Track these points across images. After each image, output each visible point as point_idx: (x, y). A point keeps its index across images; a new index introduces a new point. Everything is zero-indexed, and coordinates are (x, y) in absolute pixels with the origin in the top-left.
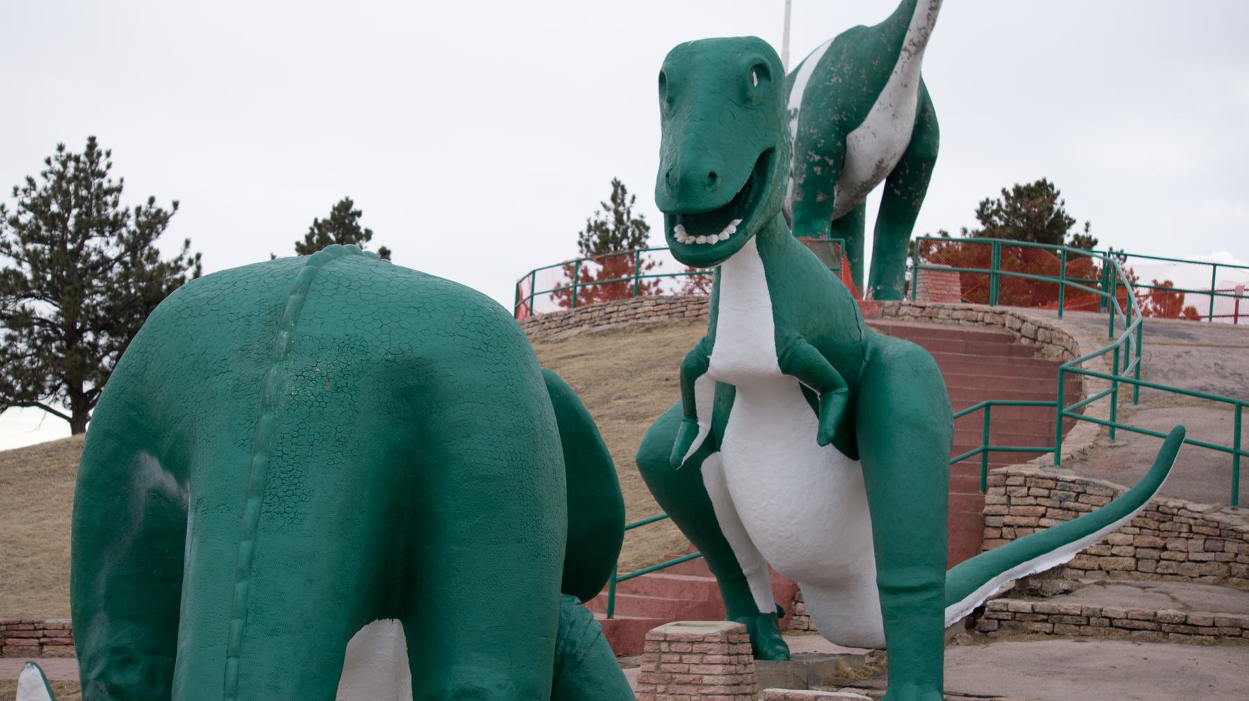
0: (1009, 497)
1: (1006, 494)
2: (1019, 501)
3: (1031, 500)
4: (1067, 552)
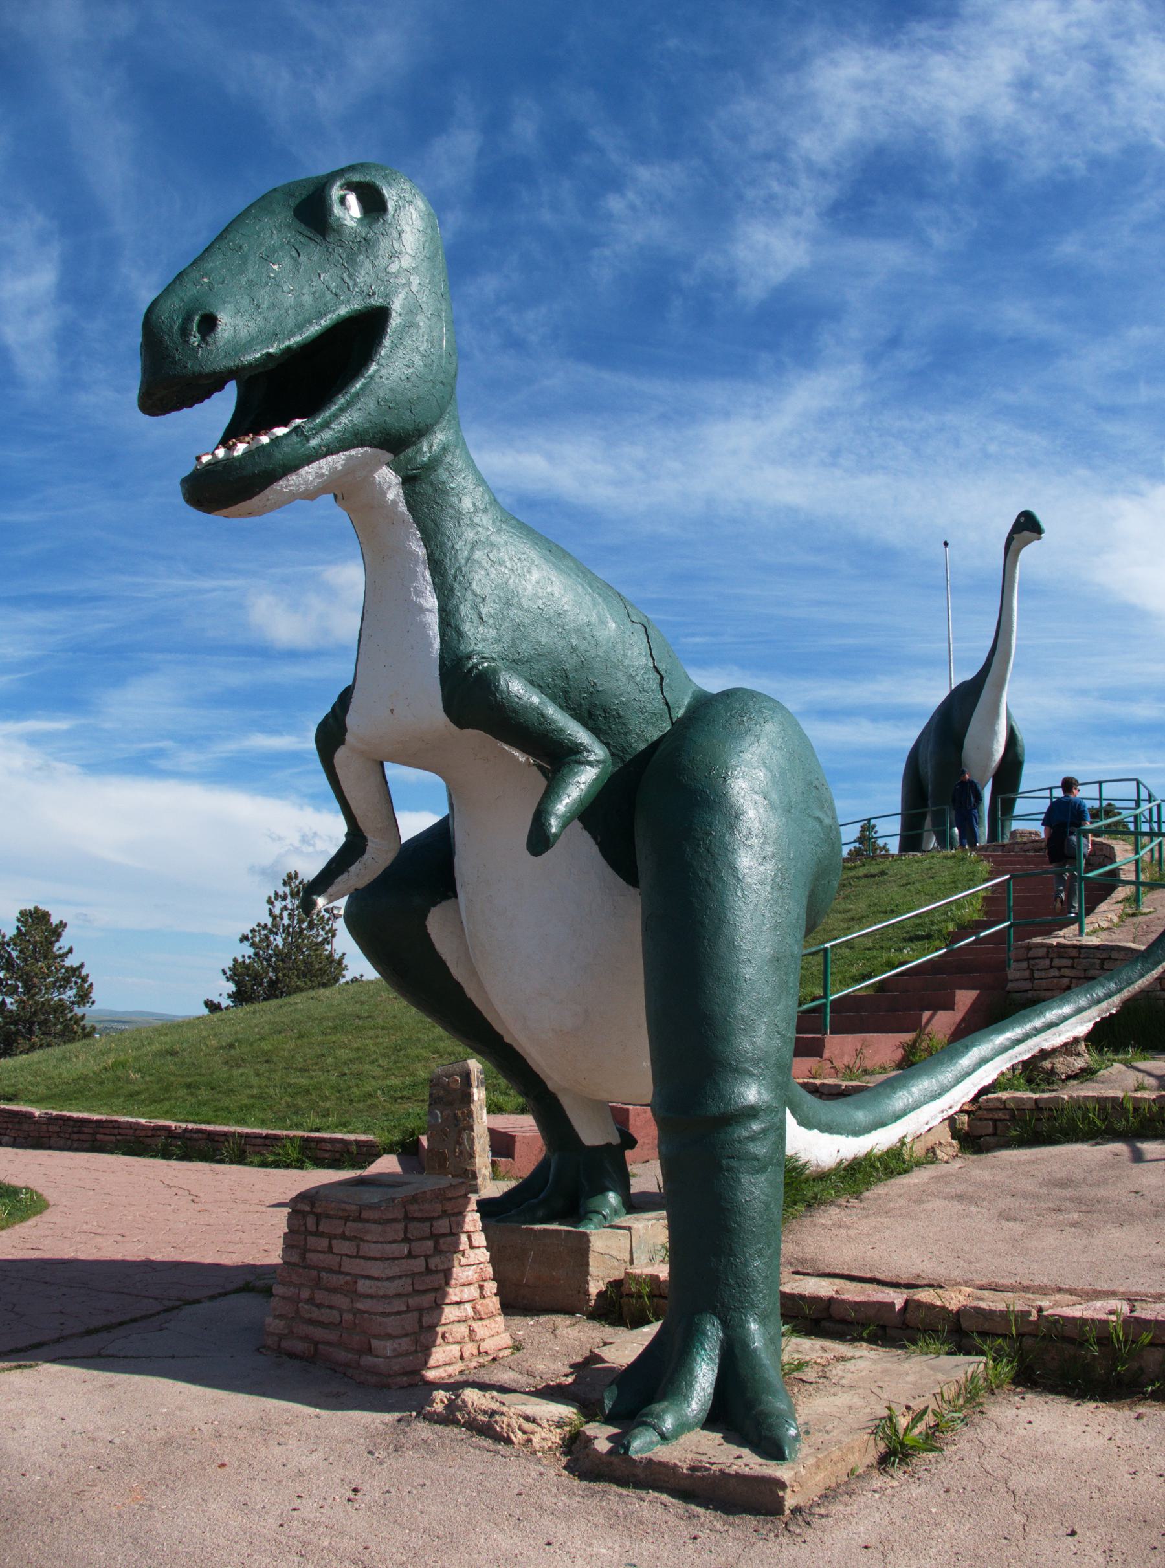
0: (1032, 970)
1: (1028, 968)
2: (1043, 974)
3: (1054, 972)
4: (1082, 1023)
